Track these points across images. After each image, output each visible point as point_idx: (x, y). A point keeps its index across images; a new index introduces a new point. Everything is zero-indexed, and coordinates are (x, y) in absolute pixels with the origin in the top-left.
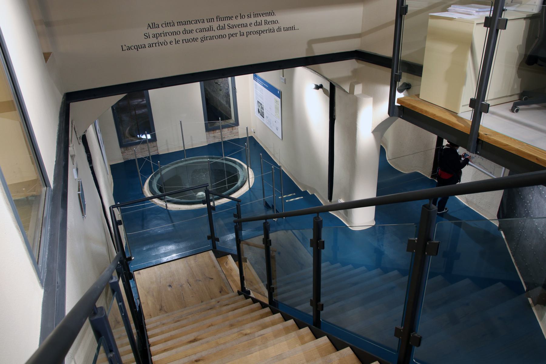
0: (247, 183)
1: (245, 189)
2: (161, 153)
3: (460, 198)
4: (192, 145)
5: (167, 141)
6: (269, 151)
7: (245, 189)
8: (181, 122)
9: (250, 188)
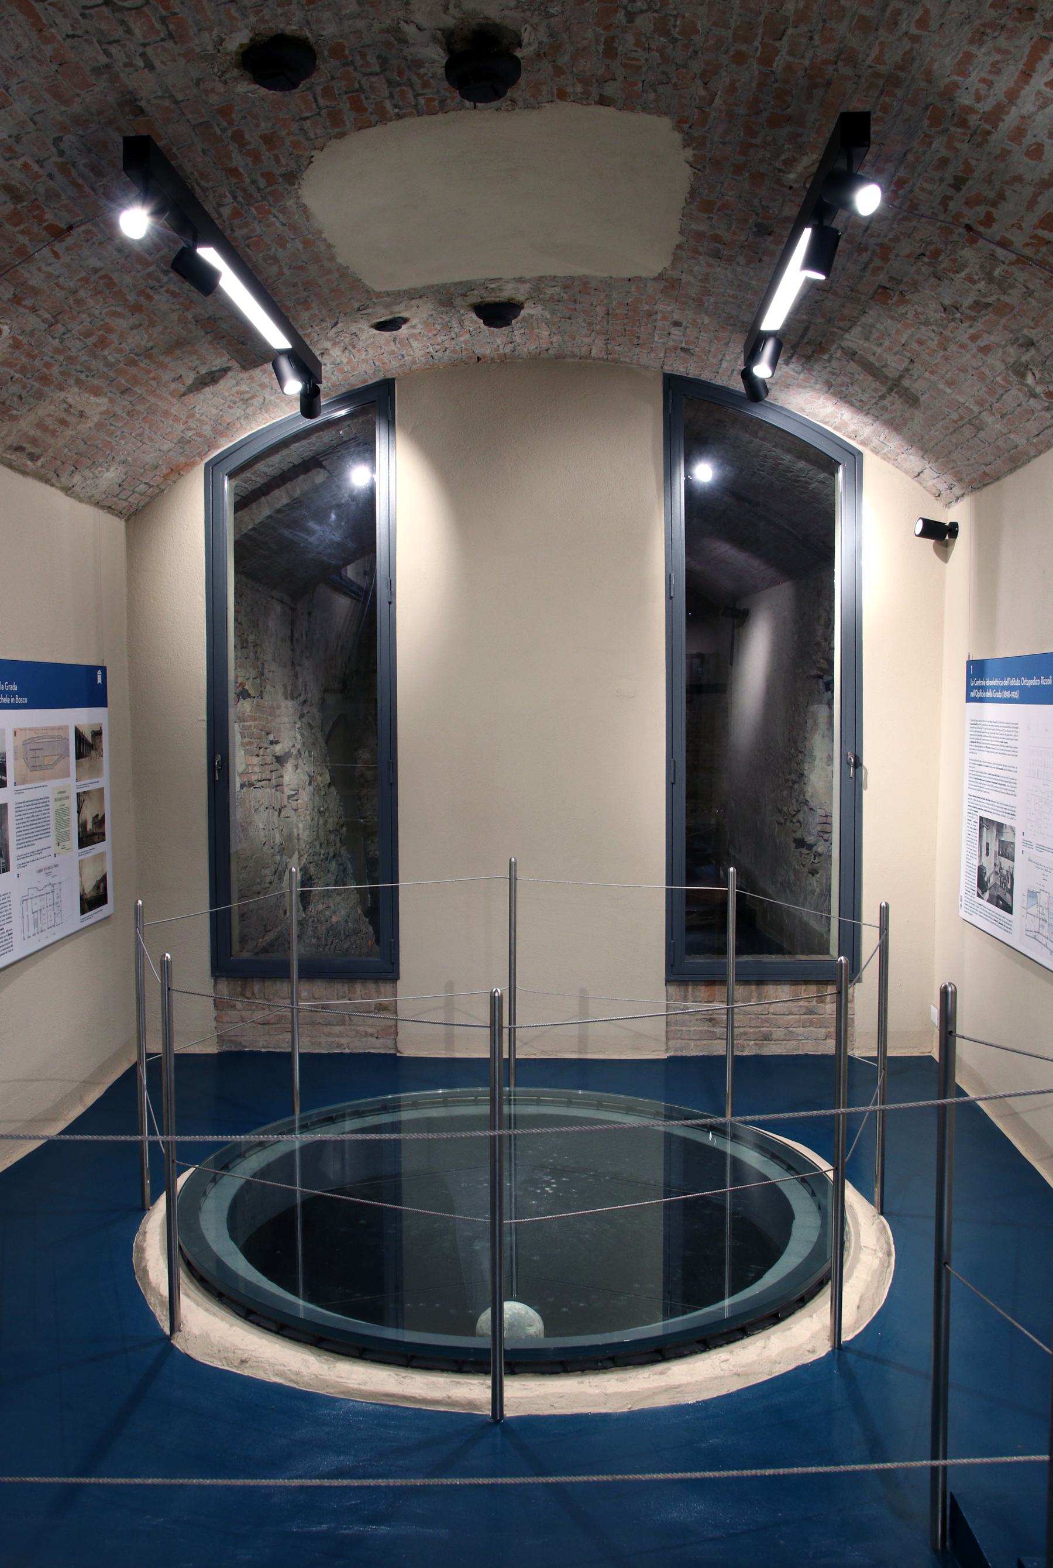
0: (822, 1304)
1: (798, 1340)
2: (408, 1051)
3: (489, 1311)
4: (583, 1042)
5: (450, 986)
6: (1029, 1134)
7: (798, 1340)
8: (512, 867)
9: (839, 1348)
